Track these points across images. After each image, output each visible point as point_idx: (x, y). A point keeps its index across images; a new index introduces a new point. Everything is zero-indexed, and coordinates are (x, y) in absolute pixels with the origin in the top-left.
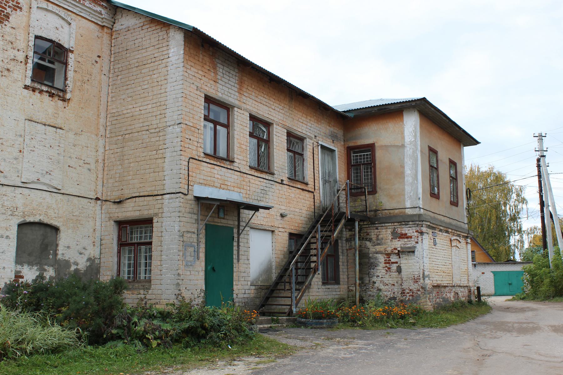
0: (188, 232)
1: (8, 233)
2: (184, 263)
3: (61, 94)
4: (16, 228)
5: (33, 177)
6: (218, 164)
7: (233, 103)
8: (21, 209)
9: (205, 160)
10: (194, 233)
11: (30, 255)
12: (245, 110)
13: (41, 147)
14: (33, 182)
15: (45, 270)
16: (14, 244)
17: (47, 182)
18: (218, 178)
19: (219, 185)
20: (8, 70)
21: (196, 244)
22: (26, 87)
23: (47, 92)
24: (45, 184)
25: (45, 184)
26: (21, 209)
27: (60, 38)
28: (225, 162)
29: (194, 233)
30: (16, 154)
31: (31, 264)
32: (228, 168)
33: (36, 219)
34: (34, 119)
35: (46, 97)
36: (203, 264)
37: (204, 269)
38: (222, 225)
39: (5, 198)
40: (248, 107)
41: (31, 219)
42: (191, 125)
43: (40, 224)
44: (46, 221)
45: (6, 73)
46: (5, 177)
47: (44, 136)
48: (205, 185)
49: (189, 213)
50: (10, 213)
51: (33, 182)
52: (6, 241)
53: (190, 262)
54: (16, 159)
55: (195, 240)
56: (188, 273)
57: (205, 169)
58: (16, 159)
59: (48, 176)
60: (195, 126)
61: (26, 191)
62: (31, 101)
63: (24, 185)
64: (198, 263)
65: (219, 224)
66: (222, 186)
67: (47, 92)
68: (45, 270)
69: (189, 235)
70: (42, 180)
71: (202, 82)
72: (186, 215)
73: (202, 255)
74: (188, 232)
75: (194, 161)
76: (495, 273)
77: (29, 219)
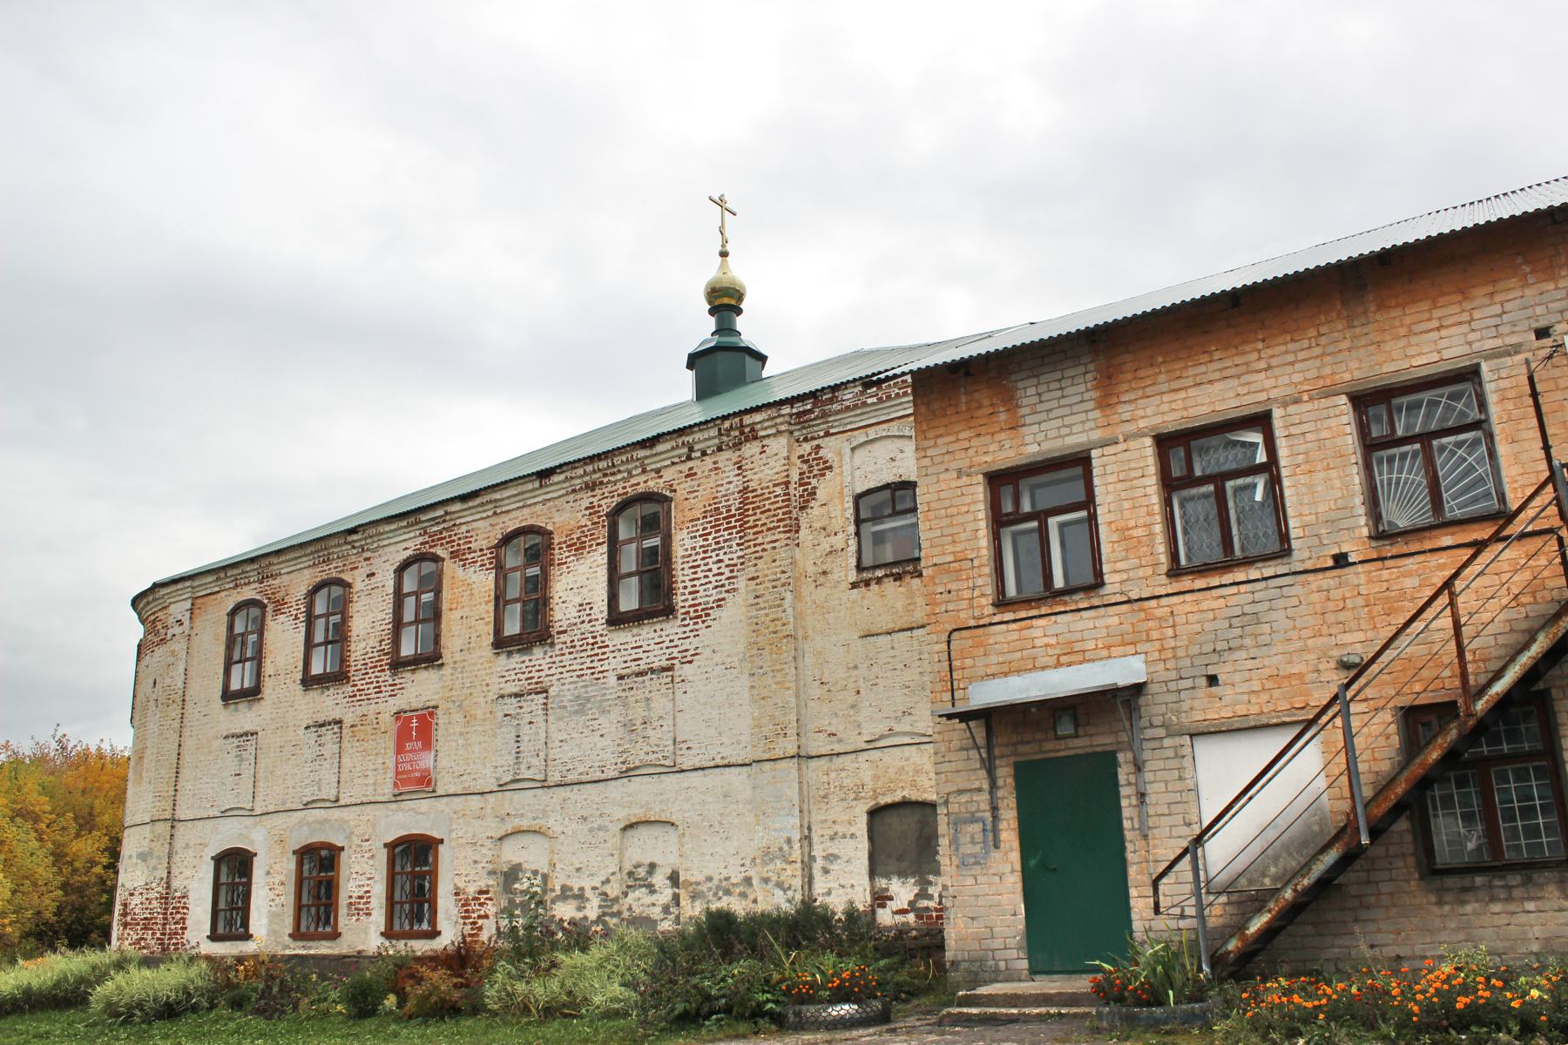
0: (960, 792)
1: (853, 830)
2: (955, 861)
3: (910, 568)
4: (864, 818)
5: (881, 728)
6: (1044, 611)
7: (1081, 444)
8: (870, 785)
9: (996, 619)
10: (979, 790)
11: (900, 859)
12: (1139, 434)
13: (889, 674)
14: (882, 737)
15: (930, 883)
16: (864, 845)
17: (907, 728)
18: (1047, 645)
19: (1052, 661)
20: (824, 573)
21: (988, 815)
22: (854, 585)
23: (886, 576)
24: (905, 734)
25: (905, 734)
26: (870, 785)
27: (901, 471)
28: (1067, 598)
29: (979, 790)
30: (850, 697)
31: (903, 874)
32: (1079, 610)
33: (897, 797)
34: (875, 630)
35: (889, 585)
36: (1015, 856)
37: (1018, 867)
38: (1071, 753)
39: (843, 774)
40: (1142, 424)
41: (888, 799)
42: (950, 558)
43: (905, 804)
44: (915, 796)
45: (821, 579)
46: (840, 741)
47: (892, 653)
48: (1006, 674)
49: (962, 749)
50: (853, 796)
51: (882, 737)
52: (852, 842)
53: (974, 855)
54: (853, 707)
55: (985, 806)
56: (970, 881)
57: (999, 638)
58: (853, 707)
59: (908, 719)
60: (960, 556)
61: (875, 755)
62: (865, 603)
63: (872, 745)
64: (996, 855)
65: (1062, 754)
66: (1063, 659)
67: (886, 576)
68: (930, 883)
69: (964, 798)
70: (897, 728)
71: (971, 452)
72: (950, 756)
73: (1009, 836)
74: (960, 792)
75: (964, 633)
76: (247, 937)
77: (883, 800)
